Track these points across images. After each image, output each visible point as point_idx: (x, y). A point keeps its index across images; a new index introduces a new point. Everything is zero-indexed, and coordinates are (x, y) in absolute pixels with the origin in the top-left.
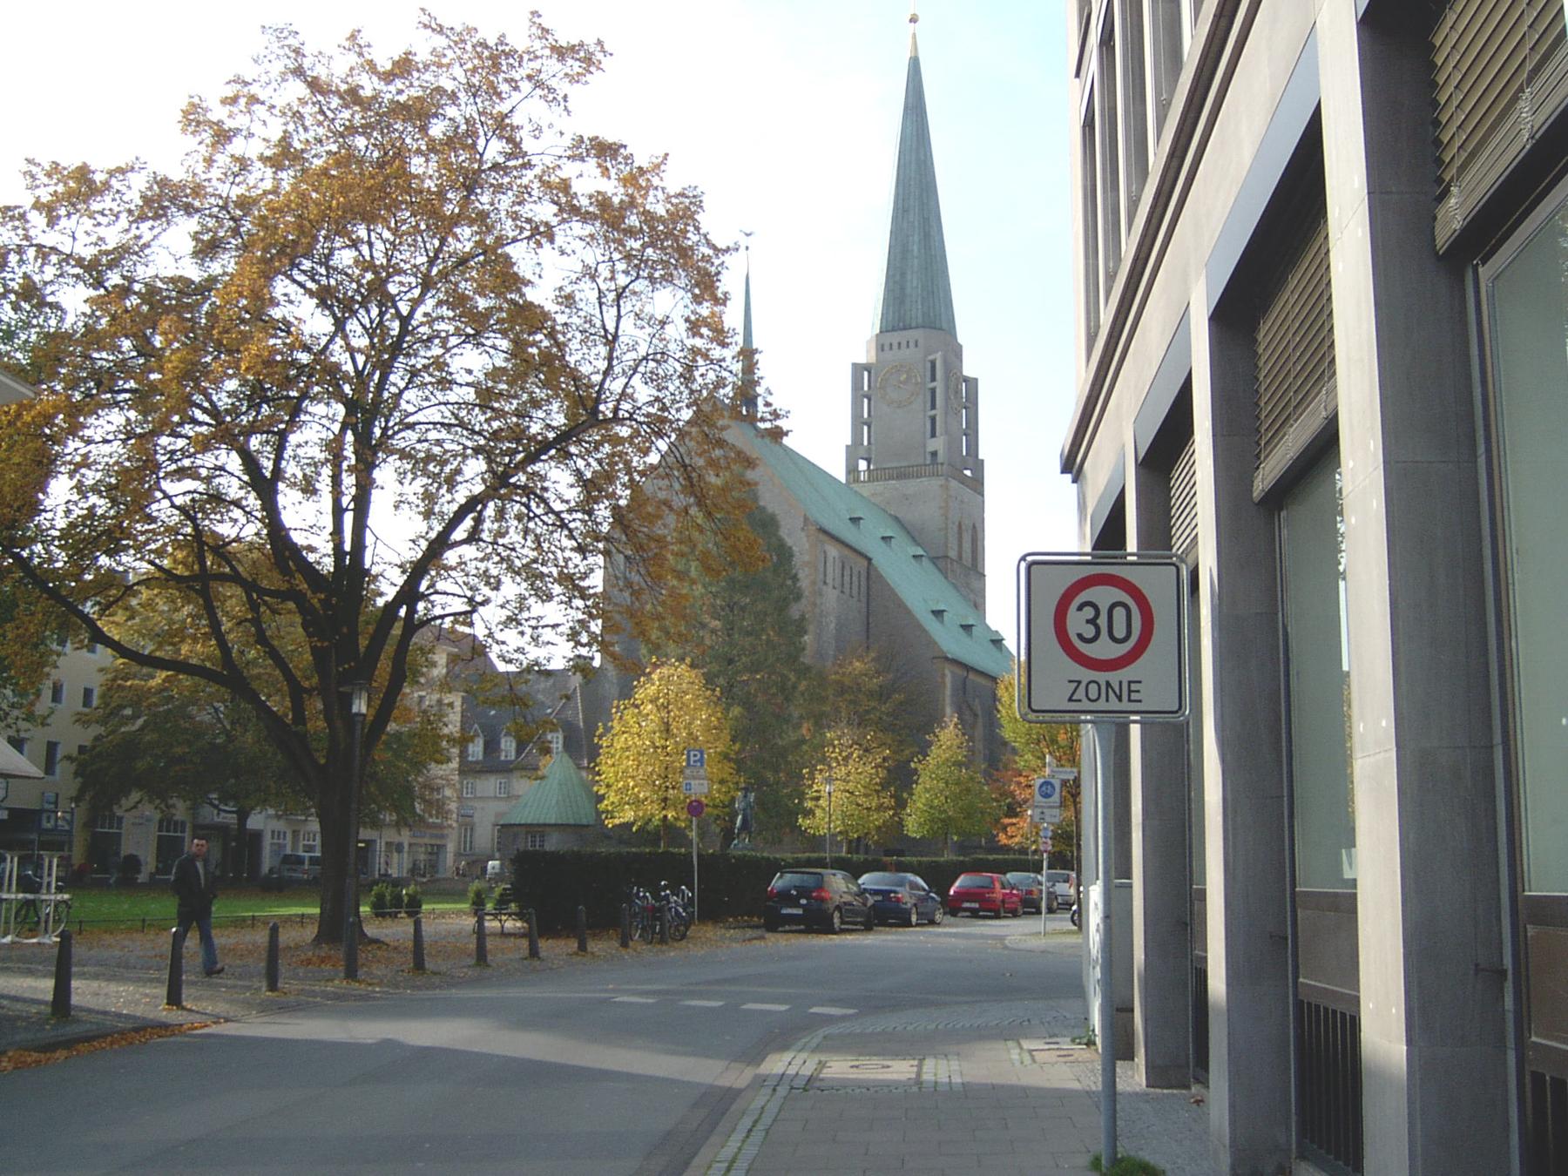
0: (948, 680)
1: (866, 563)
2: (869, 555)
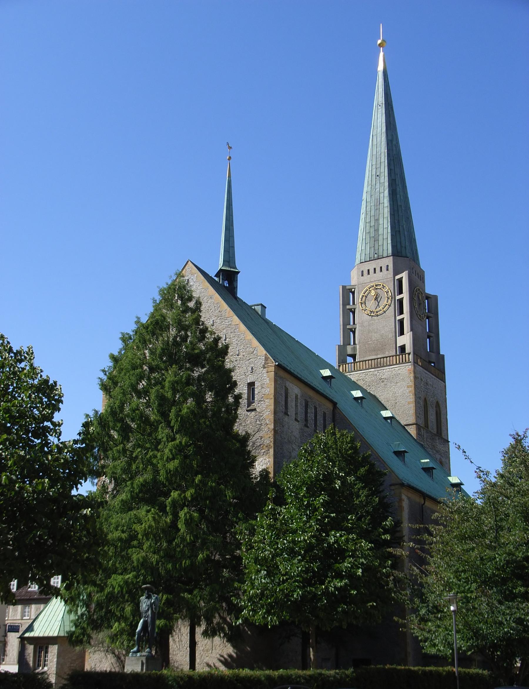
0: (405, 504)
1: (330, 406)
2: (335, 400)
